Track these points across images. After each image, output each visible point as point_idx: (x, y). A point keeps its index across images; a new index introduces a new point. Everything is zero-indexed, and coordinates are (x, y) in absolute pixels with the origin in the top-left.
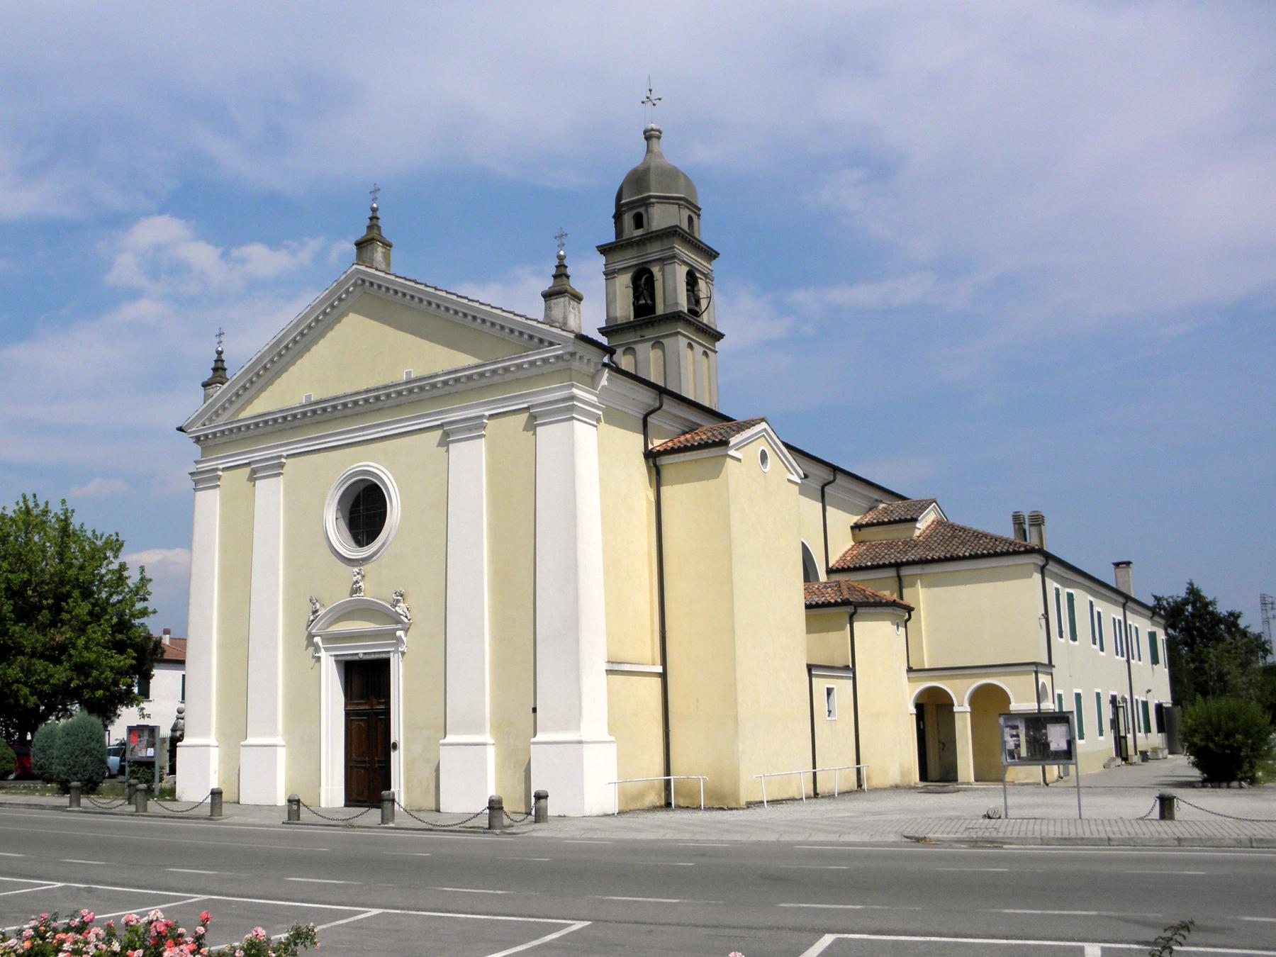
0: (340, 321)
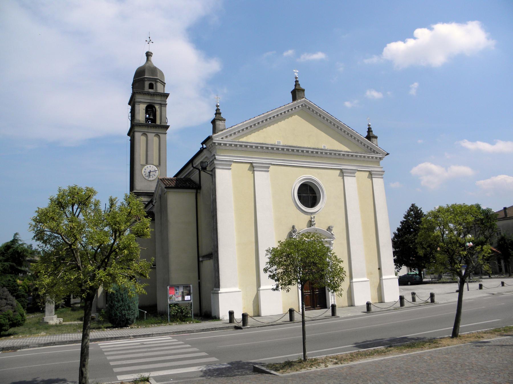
0: (292, 117)
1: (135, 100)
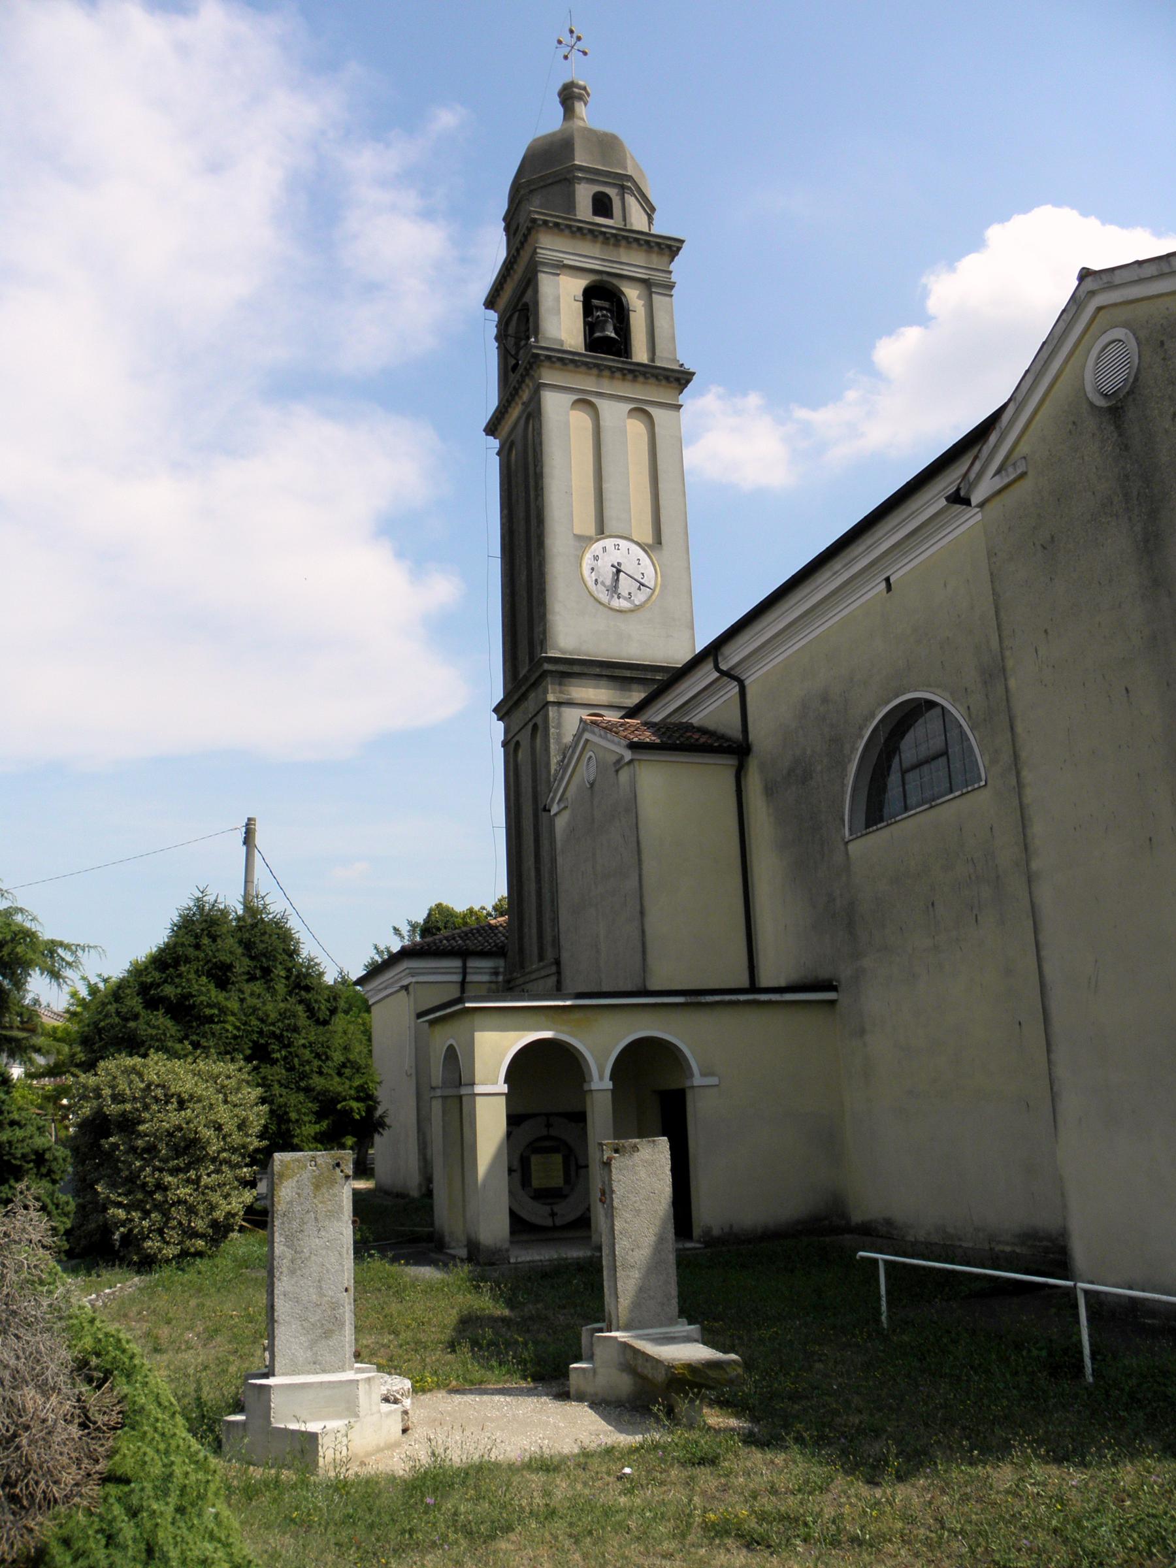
1: (535, 253)
